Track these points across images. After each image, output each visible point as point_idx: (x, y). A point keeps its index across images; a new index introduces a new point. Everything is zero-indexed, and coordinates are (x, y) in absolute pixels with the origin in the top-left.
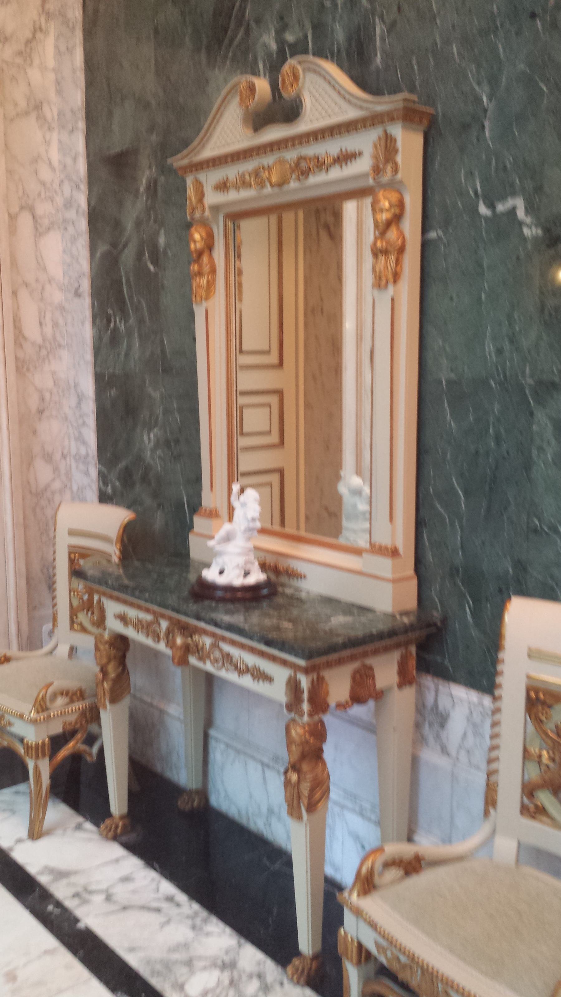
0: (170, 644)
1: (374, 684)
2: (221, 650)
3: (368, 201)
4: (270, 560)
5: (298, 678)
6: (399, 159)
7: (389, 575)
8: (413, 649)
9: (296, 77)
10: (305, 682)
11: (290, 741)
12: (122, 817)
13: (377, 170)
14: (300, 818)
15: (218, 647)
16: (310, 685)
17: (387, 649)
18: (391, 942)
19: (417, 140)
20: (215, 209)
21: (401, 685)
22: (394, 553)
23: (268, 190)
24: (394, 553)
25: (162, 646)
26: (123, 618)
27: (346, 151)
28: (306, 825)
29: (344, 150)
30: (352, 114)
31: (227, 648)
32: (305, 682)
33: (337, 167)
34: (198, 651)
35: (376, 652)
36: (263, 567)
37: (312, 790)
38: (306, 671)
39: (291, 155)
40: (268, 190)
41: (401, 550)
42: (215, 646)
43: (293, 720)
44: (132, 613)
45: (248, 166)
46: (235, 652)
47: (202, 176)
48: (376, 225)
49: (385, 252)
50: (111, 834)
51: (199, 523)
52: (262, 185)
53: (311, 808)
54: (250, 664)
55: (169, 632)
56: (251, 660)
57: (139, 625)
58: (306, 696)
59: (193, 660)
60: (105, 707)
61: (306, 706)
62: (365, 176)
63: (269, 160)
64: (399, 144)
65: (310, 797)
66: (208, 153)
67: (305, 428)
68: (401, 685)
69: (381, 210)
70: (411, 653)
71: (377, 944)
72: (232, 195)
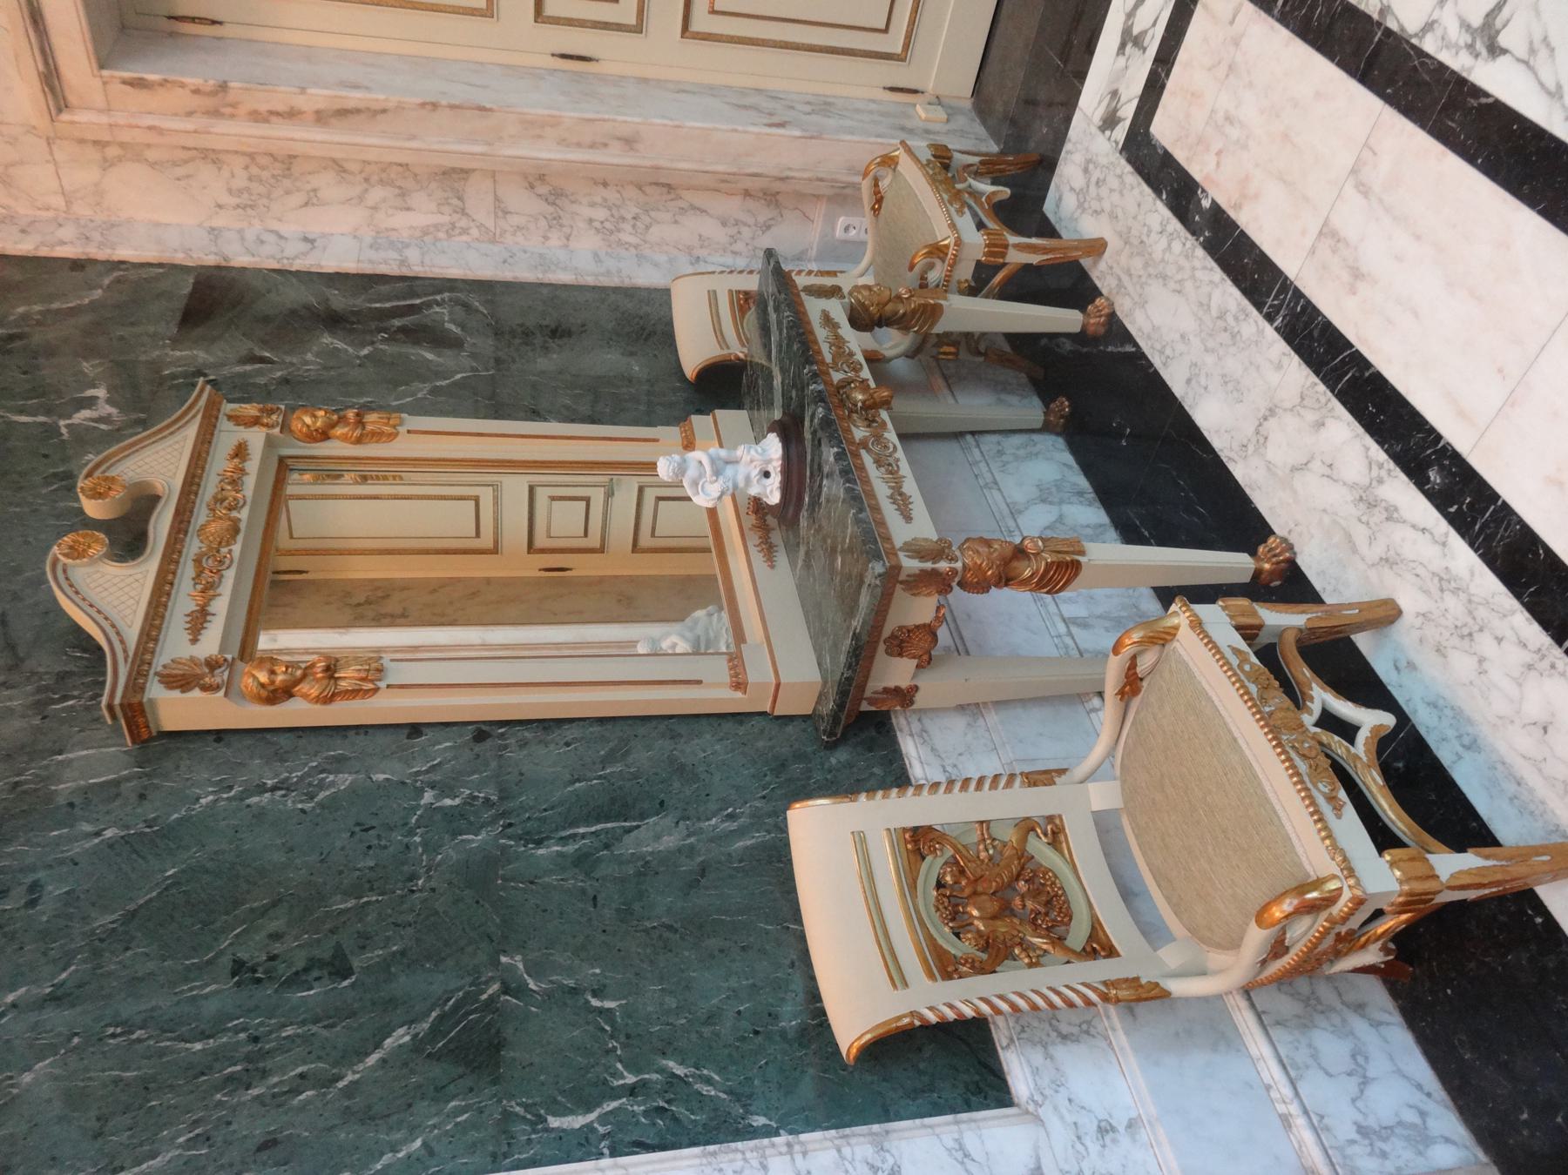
45: (187, 571)
66: (132, 635)
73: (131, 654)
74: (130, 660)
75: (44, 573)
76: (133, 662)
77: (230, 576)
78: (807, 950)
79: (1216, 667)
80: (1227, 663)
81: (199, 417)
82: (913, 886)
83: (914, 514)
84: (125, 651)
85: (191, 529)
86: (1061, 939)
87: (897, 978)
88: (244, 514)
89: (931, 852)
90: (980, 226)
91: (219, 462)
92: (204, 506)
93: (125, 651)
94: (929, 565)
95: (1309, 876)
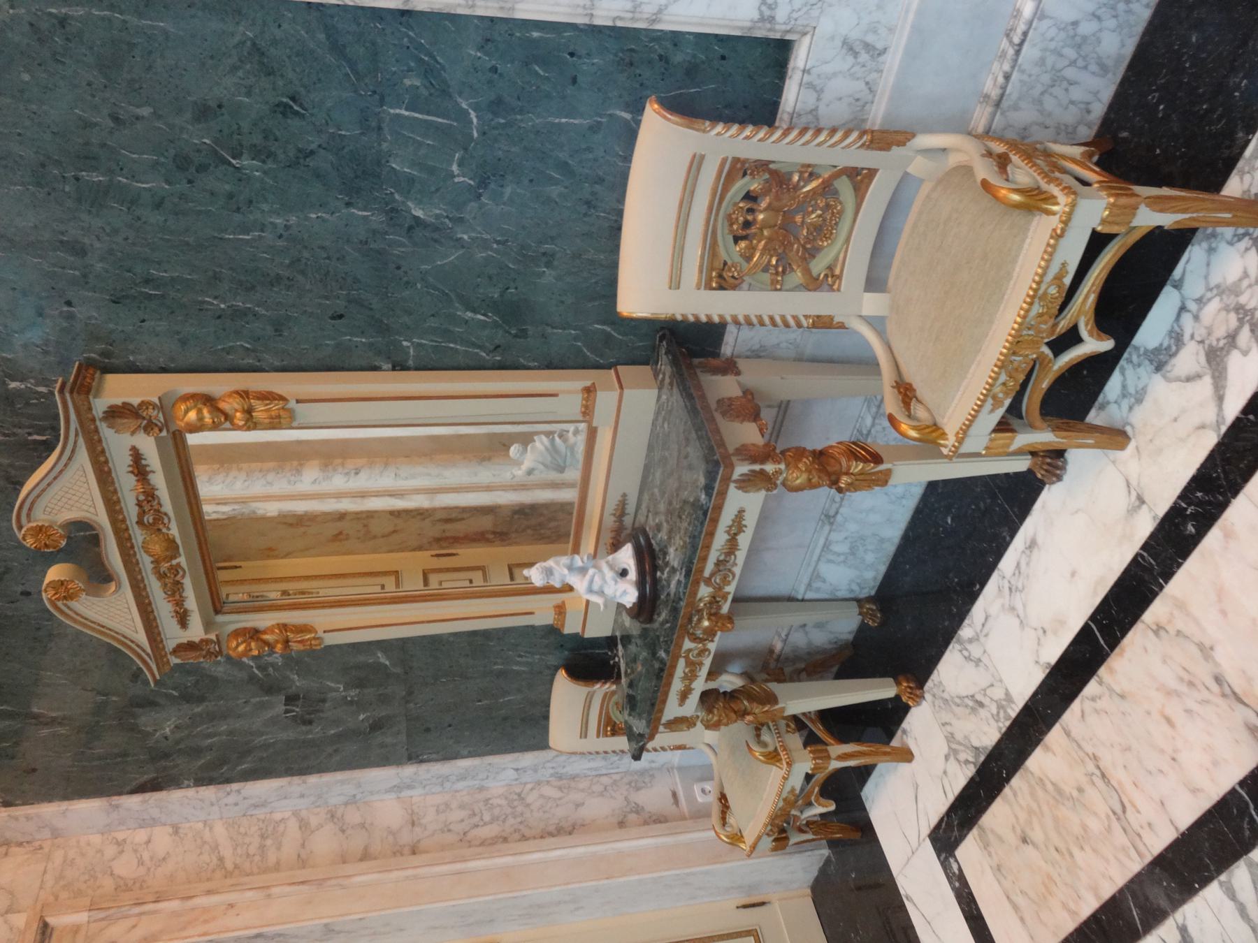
0: (710, 633)
1: (737, 398)
2: (713, 574)
3: (193, 439)
4: (607, 538)
5: (872, 114)
6: (135, 401)
7: (615, 394)
8: (696, 361)
9: (40, 529)
10: (742, 469)
11: (810, 485)
12: (898, 683)
13: (149, 427)
14: (888, 473)
15: (710, 579)
16: (747, 462)
17: (699, 387)
18: (989, 394)
19: (112, 380)
20: (208, 625)
21: (738, 373)
22: (589, 391)
23: (182, 560)
24: (589, 391)
25: (712, 646)
26: (684, 696)
27: (130, 466)
28: (894, 465)
29: (131, 469)
30: (83, 457)
31: (709, 567)
32: (742, 469)
33: (151, 476)
34: (714, 601)
35: (703, 397)
36: (616, 546)
37: (857, 458)
38: (731, 467)
39: (138, 535)
40: (182, 560)
41: (588, 383)
42: (708, 582)
43: (784, 484)
44: (677, 685)
45: (155, 588)
46: (713, 557)
47: (170, 645)
48: (215, 427)
49: (249, 412)
50: (918, 692)
51: (571, 627)
52: (176, 569)
53: (877, 459)
54: (727, 537)
55: (695, 639)
56: (720, 538)
57: (690, 677)
58: (757, 467)
59: (725, 609)
60: (783, 710)
61: (770, 468)
62: (160, 443)
63: (146, 562)
64: (118, 401)
65: (865, 461)
66: (142, 637)
67: (455, 634)
68: (738, 373)
69: (201, 419)
70: (700, 363)
71: (992, 411)
72: (191, 603)
73: (149, 650)
74: (152, 657)
75: (11, 525)
76: (155, 657)
77: (187, 582)
78: (619, 229)
79: (963, 420)
80: (1046, 269)
81: (81, 441)
82: (725, 189)
83: (688, 701)
84: (148, 655)
85: (136, 549)
86: (820, 226)
87: (675, 282)
88: (174, 531)
89: (751, 174)
90: (808, 777)
91: (127, 484)
92: (136, 527)
93: (148, 655)
94: (757, 467)
95: (943, 417)
